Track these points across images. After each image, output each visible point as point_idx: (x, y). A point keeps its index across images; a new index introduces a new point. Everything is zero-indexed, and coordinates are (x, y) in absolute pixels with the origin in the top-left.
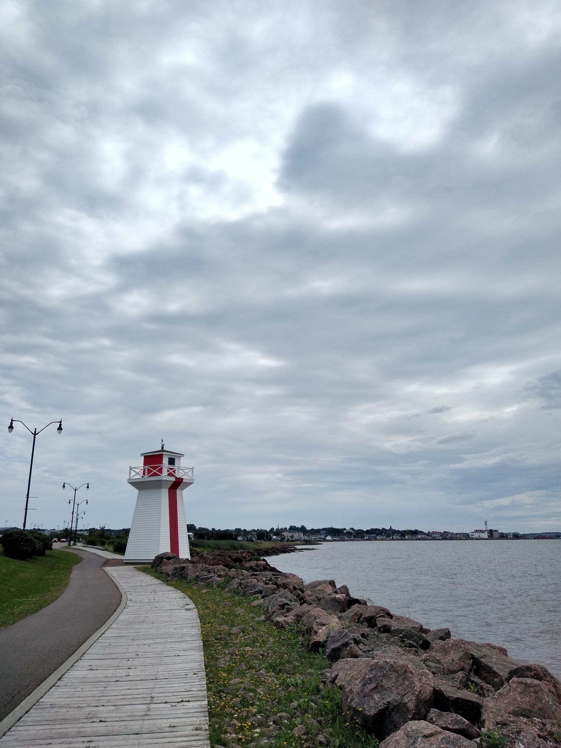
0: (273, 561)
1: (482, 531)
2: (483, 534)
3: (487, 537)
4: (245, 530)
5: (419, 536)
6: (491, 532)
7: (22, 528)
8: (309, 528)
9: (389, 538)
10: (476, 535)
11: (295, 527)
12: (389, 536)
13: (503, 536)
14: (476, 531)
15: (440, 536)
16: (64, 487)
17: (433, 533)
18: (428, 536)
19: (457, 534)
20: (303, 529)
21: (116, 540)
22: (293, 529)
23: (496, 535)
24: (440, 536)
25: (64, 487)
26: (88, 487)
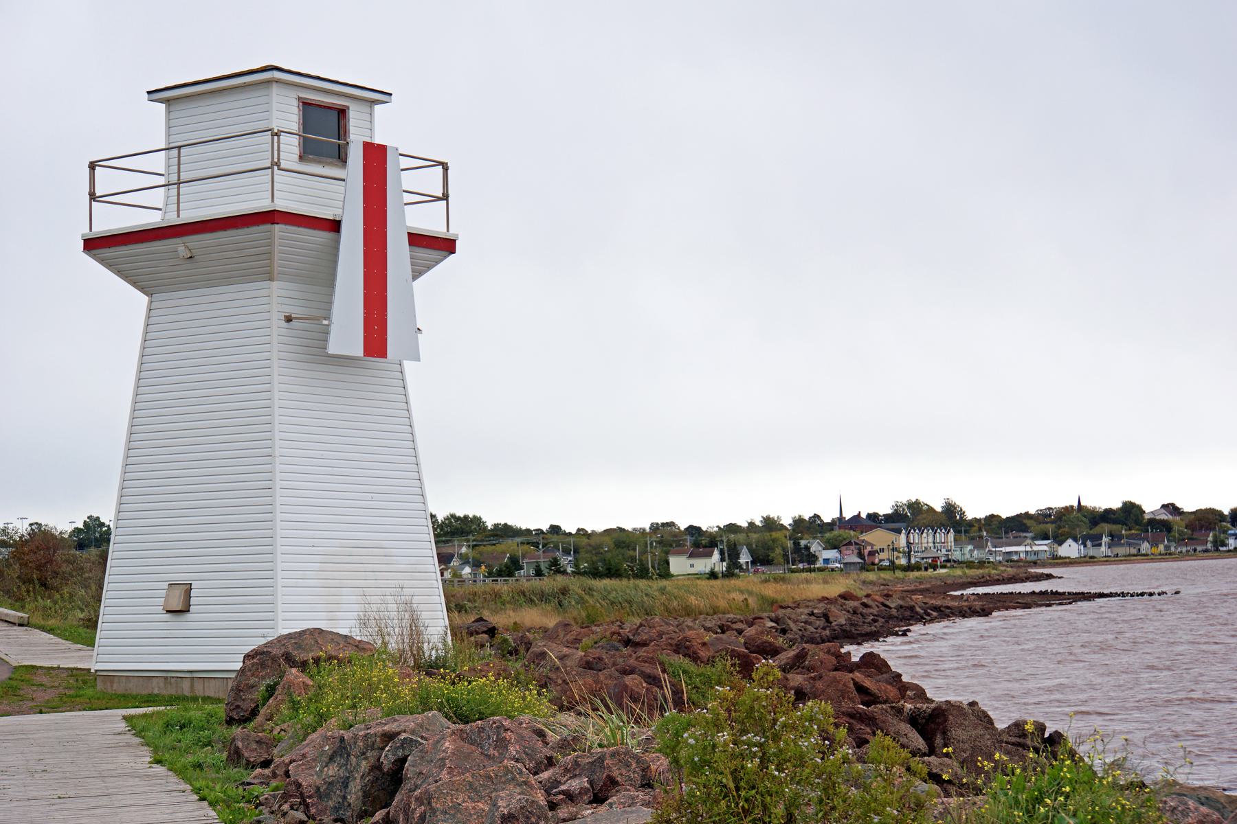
0: (889, 649)
4: (693, 530)
8: (974, 510)
11: (555, 529)
20: (951, 518)
22: (910, 517)
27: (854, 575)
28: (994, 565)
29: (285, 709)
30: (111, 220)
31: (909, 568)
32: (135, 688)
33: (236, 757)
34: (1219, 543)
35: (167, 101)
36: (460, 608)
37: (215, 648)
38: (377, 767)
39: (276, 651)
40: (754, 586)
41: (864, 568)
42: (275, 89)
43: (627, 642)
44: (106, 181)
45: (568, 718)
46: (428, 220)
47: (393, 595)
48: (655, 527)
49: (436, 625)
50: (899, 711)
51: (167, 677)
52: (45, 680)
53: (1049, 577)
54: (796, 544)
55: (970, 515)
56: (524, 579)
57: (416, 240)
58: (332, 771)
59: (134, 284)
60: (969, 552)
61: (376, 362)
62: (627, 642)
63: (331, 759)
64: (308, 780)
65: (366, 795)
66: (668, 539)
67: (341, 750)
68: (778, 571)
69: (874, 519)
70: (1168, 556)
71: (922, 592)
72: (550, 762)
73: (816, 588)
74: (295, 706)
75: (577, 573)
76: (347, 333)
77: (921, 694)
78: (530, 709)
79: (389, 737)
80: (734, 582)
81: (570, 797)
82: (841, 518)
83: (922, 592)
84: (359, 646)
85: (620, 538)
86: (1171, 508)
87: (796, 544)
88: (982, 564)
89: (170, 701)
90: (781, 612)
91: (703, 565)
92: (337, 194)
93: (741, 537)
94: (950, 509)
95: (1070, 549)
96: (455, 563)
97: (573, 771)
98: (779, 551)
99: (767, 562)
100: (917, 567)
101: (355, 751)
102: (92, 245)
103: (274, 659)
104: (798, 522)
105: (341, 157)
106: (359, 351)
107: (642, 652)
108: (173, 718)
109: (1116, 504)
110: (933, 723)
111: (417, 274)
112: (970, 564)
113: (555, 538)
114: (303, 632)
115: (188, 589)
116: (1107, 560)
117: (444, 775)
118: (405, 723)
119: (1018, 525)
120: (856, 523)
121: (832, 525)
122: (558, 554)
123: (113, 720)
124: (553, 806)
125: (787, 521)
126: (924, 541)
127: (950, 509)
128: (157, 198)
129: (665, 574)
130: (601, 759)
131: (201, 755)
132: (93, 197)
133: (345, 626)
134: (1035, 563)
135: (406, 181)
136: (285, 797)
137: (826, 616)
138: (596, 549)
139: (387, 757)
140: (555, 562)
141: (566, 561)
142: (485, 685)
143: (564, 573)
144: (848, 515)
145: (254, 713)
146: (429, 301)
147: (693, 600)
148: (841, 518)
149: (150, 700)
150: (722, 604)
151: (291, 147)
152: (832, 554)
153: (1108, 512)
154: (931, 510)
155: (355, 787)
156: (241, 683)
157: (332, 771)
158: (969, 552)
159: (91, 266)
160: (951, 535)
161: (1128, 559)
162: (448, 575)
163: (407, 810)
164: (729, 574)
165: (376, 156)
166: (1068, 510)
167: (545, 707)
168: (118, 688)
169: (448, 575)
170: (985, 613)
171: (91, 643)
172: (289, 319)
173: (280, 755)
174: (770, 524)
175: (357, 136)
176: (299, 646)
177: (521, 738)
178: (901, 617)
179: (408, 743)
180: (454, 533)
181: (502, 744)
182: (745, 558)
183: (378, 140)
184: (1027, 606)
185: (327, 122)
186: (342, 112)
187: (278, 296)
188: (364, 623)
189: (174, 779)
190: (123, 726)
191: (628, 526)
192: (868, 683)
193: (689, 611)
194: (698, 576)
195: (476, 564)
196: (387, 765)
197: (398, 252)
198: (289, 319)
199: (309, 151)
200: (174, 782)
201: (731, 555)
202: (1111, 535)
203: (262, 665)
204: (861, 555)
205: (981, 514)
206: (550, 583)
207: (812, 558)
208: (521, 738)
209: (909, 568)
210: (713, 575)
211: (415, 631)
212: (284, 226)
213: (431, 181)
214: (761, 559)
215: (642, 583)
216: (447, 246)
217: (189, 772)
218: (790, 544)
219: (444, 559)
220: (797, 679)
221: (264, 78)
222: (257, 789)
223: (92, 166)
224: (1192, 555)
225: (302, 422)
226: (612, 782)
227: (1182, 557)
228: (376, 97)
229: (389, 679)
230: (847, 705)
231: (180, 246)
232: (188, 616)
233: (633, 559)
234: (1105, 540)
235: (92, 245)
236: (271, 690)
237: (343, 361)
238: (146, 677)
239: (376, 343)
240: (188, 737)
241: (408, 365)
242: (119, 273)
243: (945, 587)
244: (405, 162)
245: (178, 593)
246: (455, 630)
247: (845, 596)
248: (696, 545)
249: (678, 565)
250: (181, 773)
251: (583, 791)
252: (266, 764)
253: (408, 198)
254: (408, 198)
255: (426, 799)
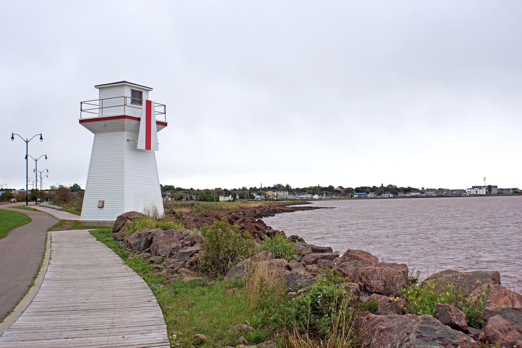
0: (264, 219)
1: (480, 187)
2: (481, 190)
3: (485, 193)
4: (225, 190)
5: (413, 194)
6: (490, 188)
7: (26, 189)
8: (293, 187)
9: (380, 196)
10: (473, 192)
11: (192, 189)
12: (380, 194)
13: (502, 192)
14: (474, 187)
15: (435, 193)
16: (13, 138)
17: (428, 190)
18: (423, 193)
19: (453, 191)
20: (288, 188)
21: (69, 197)
22: (278, 188)
23: (494, 191)
24: (435, 193)
25: (13, 138)
26: (41, 138)
27: (263, 202)
28: (297, 200)
29: (127, 229)
30: (86, 116)
31: (277, 200)
32: (90, 225)
33: (116, 239)
34: (352, 196)
35: (99, 88)
36: (167, 208)
37: (110, 216)
38: (147, 239)
39: (124, 216)
40: (239, 204)
41: (266, 200)
42: (125, 87)
43: (205, 216)
44: (84, 106)
45: (188, 231)
46: (161, 118)
47: (154, 204)
48: (216, 189)
49: (161, 211)
50: (265, 232)
51: (98, 222)
52: (68, 223)
53: (310, 203)
54: (250, 194)
55: (292, 188)
56: (183, 201)
57: (158, 123)
58: (138, 240)
59: (91, 131)
60: (292, 197)
61: (148, 151)
62: (205, 216)
63: (137, 238)
64: (132, 242)
65: (145, 245)
66: (219, 192)
67: (140, 236)
68: (245, 200)
69: (269, 188)
70: (339, 199)
71: (279, 206)
72: (183, 238)
73: (253, 205)
74: (129, 228)
75: (197, 200)
76: (141, 144)
77: (271, 228)
78: (180, 228)
79: (150, 233)
80: (235, 203)
81: (186, 245)
82: (261, 188)
83: (279, 206)
84: (143, 215)
85: (207, 191)
86: (341, 187)
87: (250, 194)
88: (295, 199)
89: (99, 228)
90: (244, 210)
91: (227, 199)
92: (140, 112)
93: (237, 192)
94: (288, 186)
95: (316, 197)
96: (167, 197)
97: (187, 240)
98: (246, 195)
99: (243, 198)
100: (278, 200)
101: (143, 236)
102: (81, 122)
103: (124, 218)
104: (251, 189)
105: (140, 103)
106: (145, 149)
107: (207, 218)
108: (99, 230)
109: (327, 186)
110: (272, 234)
111: (158, 131)
112: (291, 200)
113: (191, 191)
114: (131, 212)
115: (103, 202)
116: (327, 199)
117: (161, 241)
118: (153, 231)
119: (303, 191)
120: (265, 189)
121: (259, 189)
122: (192, 195)
123: (86, 231)
124: (183, 247)
125: (248, 188)
126: (281, 194)
127: (288, 186)
128: (97, 111)
129: (218, 200)
130: (193, 237)
131: (108, 239)
132: (81, 110)
133: (140, 210)
134: (307, 200)
135: (156, 109)
136: (127, 247)
137: (255, 211)
138: (202, 194)
139: (149, 237)
140: (191, 197)
141: (194, 197)
142: (171, 223)
143: (194, 200)
144: (263, 187)
145: (119, 230)
146: (160, 137)
147: (223, 207)
148: (261, 188)
149: (94, 228)
150: (230, 208)
151: (129, 100)
152: (259, 197)
153: (326, 188)
154: (283, 186)
155: (142, 244)
156: (116, 223)
157: (138, 240)
158: (292, 197)
159: (80, 126)
160: (287, 193)
161: (330, 199)
162: (165, 200)
163: (153, 248)
164: (233, 201)
165: (149, 103)
166: (316, 187)
167: (183, 228)
168: (86, 225)
169: (165, 200)
170: (293, 211)
171: (80, 215)
172: (128, 140)
173: (125, 238)
174: (244, 189)
175: (144, 99)
176: (130, 215)
177: (177, 233)
178: (272, 212)
179: (154, 234)
180: (166, 190)
181: (173, 235)
182: (238, 197)
183: (149, 100)
184: (303, 210)
185: (137, 95)
186: (141, 93)
187: (126, 135)
188: (145, 210)
189: (102, 243)
190: (88, 233)
191: (210, 189)
192: (258, 226)
193: (222, 209)
194: (226, 201)
195: (172, 197)
196: (149, 239)
197: (154, 126)
198: (128, 140)
199: (133, 102)
200: (102, 244)
201: (234, 196)
202: (326, 193)
203: (121, 219)
204: (265, 197)
205: (295, 188)
206: (190, 202)
207: (254, 197)
208: (177, 233)
209: (277, 200)
210: (229, 201)
211: (156, 212)
212: (127, 118)
213: (162, 109)
214: (241, 197)
215: (212, 203)
216: (165, 124)
217: (105, 242)
218: (249, 194)
219: (163, 196)
220: (242, 225)
221: (123, 84)
222: (121, 245)
223: (81, 103)
224: (345, 199)
225: (130, 163)
226: (195, 242)
227: (343, 199)
228: (149, 89)
229: (150, 222)
230: (253, 231)
231: (102, 123)
232: (103, 208)
233: (210, 197)
234: (325, 194)
235: (81, 122)
236: (123, 225)
237: (141, 150)
238: (93, 222)
239: (148, 146)
240: (104, 235)
241: (155, 151)
242: (88, 128)
243: (285, 205)
244: (156, 105)
245: (101, 203)
246: (165, 213)
247: (260, 207)
248: (226, 194)
249: (221, 198)
250: (104, 242)
251: (189, 244)
252: (122, 240)
253: (156, 113)
254: (156, 113)
255: (157, 245)
